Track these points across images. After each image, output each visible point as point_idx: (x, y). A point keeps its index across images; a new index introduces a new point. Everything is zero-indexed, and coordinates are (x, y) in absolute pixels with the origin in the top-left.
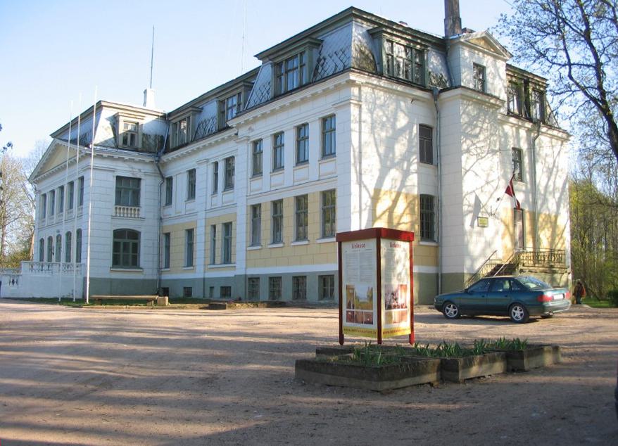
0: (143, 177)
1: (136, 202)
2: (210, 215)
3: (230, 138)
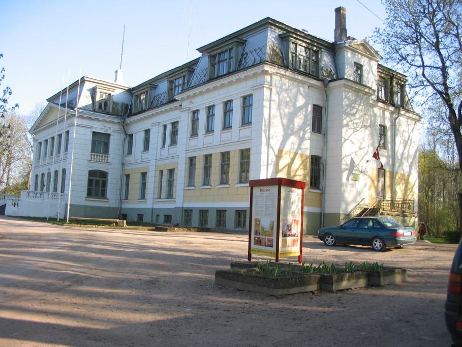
1: (106, 151)
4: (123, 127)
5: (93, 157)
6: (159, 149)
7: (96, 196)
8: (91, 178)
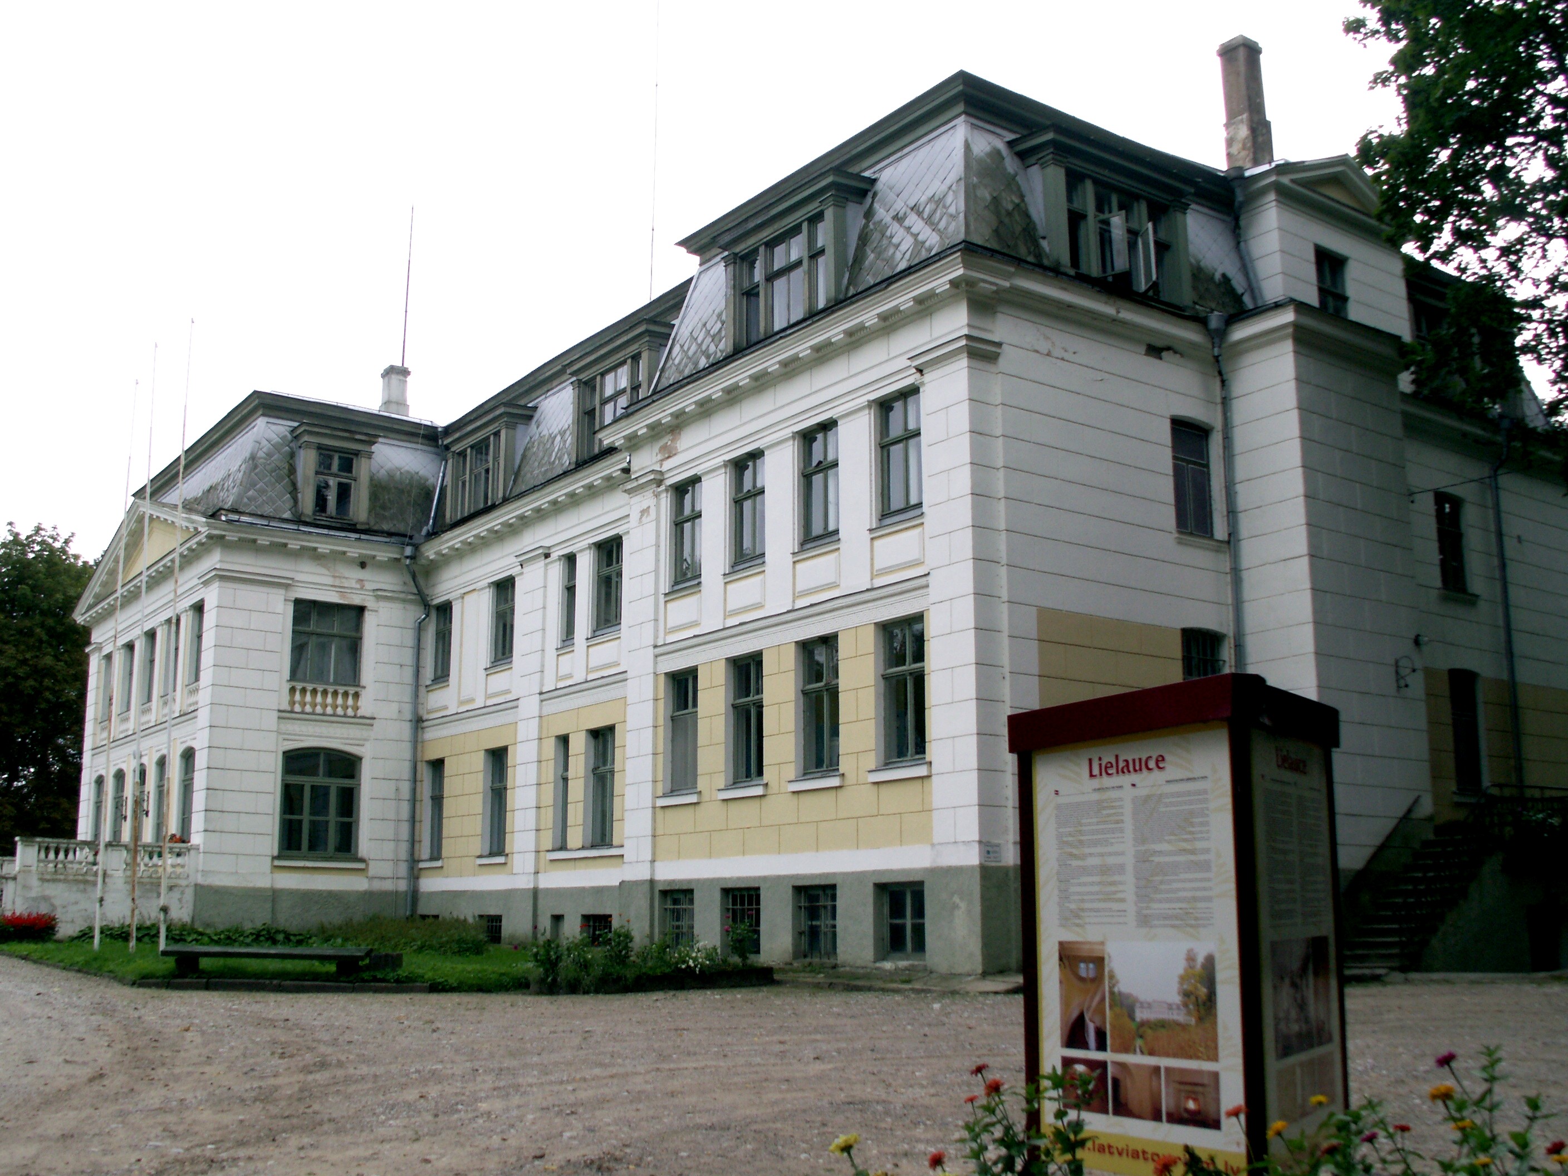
0: (369, 603)
1: (351, 674)
2: (553, 707)
3: (611, 484)
4: (414, 578)
5: (298, 697)
6: (551, 653)
7: (316, 845)
8: (296, 779)
